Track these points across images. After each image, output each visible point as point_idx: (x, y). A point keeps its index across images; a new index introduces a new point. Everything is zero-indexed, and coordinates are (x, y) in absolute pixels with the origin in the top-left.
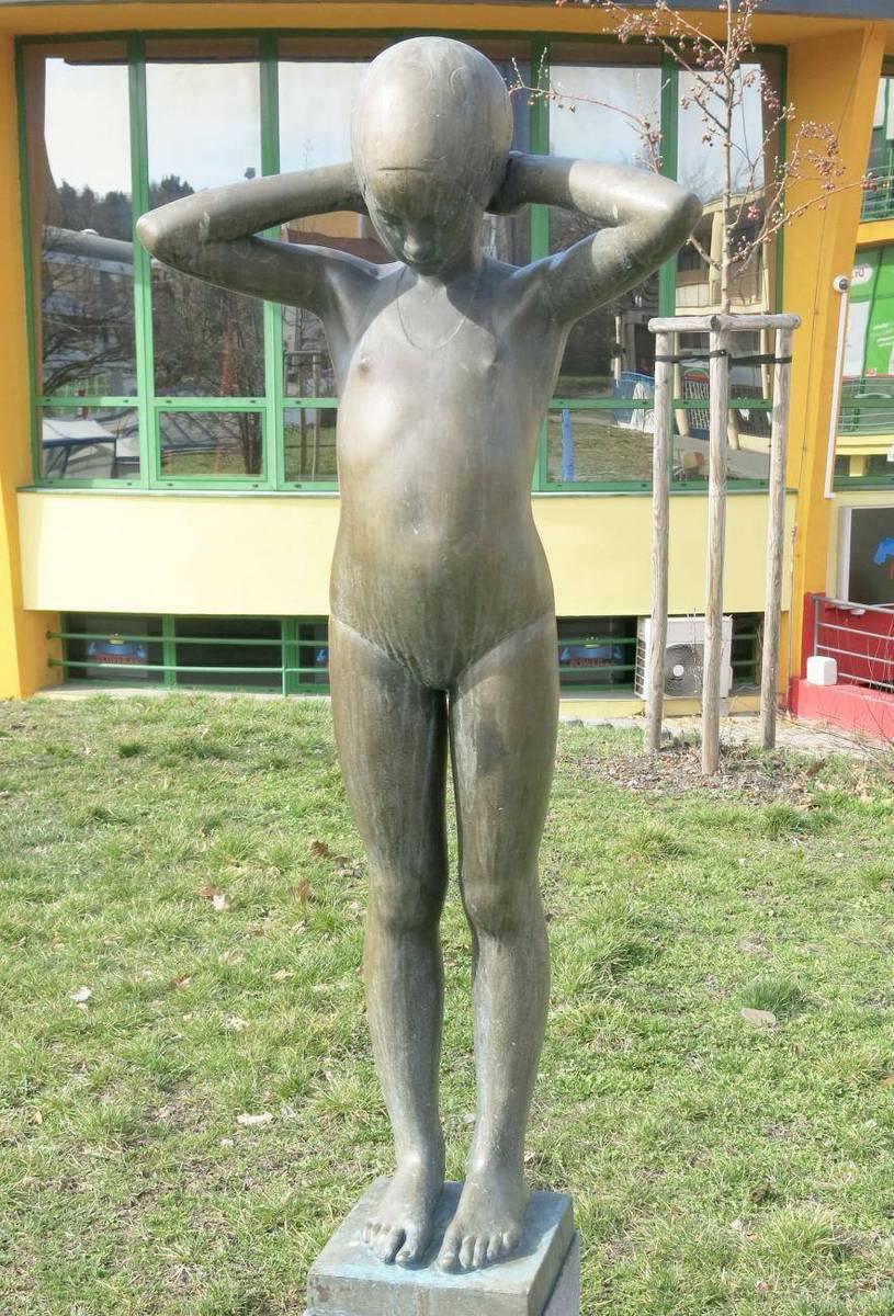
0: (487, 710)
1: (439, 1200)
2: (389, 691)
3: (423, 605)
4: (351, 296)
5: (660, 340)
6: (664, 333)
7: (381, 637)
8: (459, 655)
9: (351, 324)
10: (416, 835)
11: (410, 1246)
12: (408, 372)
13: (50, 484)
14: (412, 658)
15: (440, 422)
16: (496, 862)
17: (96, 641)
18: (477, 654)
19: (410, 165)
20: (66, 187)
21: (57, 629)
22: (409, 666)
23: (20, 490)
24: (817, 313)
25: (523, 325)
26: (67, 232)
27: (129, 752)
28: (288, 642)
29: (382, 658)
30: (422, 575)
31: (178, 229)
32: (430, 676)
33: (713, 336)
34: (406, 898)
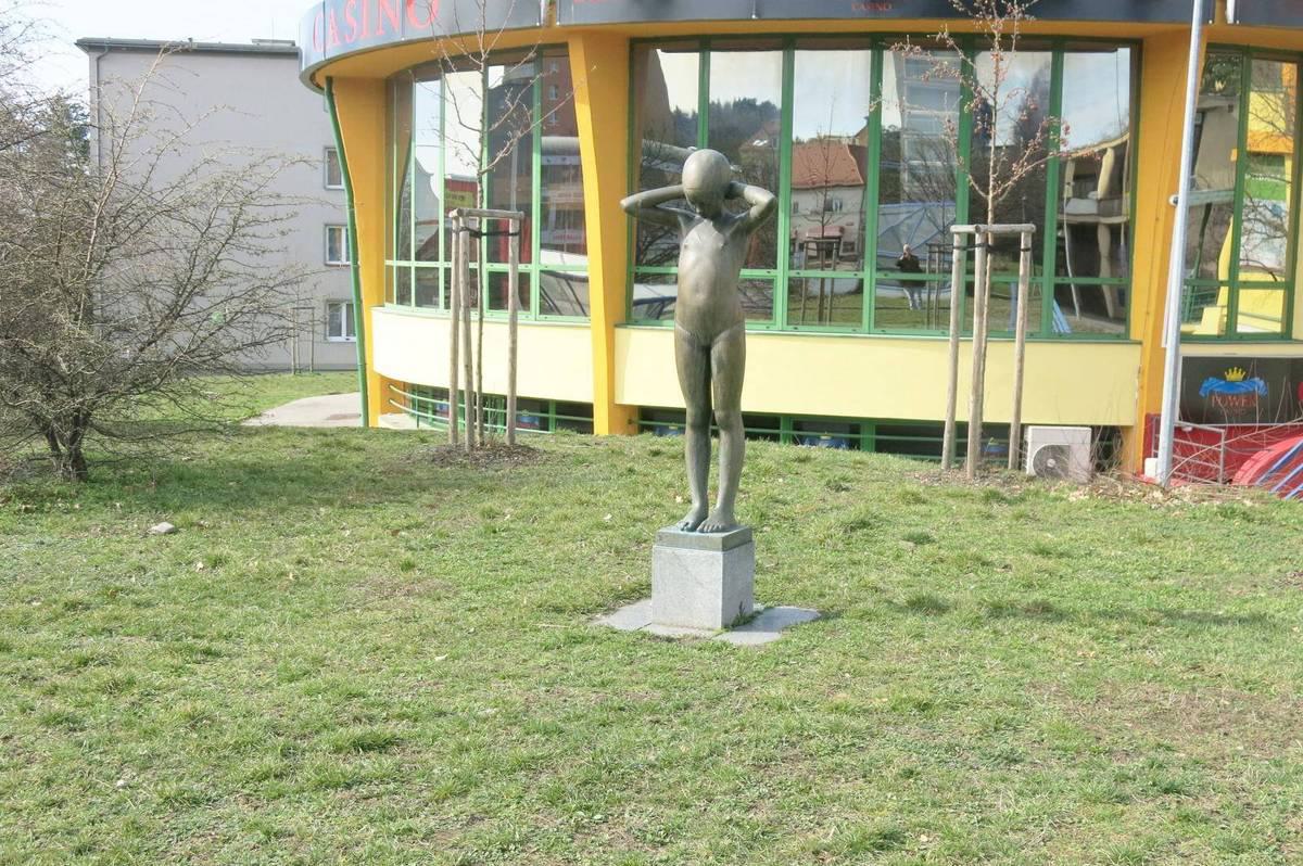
0: (720, 353)
1: (702, 516)
4: (685, 224)
5: (956, 237)
6: (958, 233)
9: (684, 234)
10: (699, 394)
11: (689, 526)
12: (699, 248)
13: (636, 323)
15: (707, 263)
17: (660, 426)
18: (717, 335)
20: (678, 111)
21: (635, 418)
23: (616, 326)
24: (1157, 219)
25: (734, 235)
26: (676, 148)
27: (656, 453)
28: (785, 432)
30: (699, 309)
32: (703, 342)
33: (977, 236)
34: (696, 416)
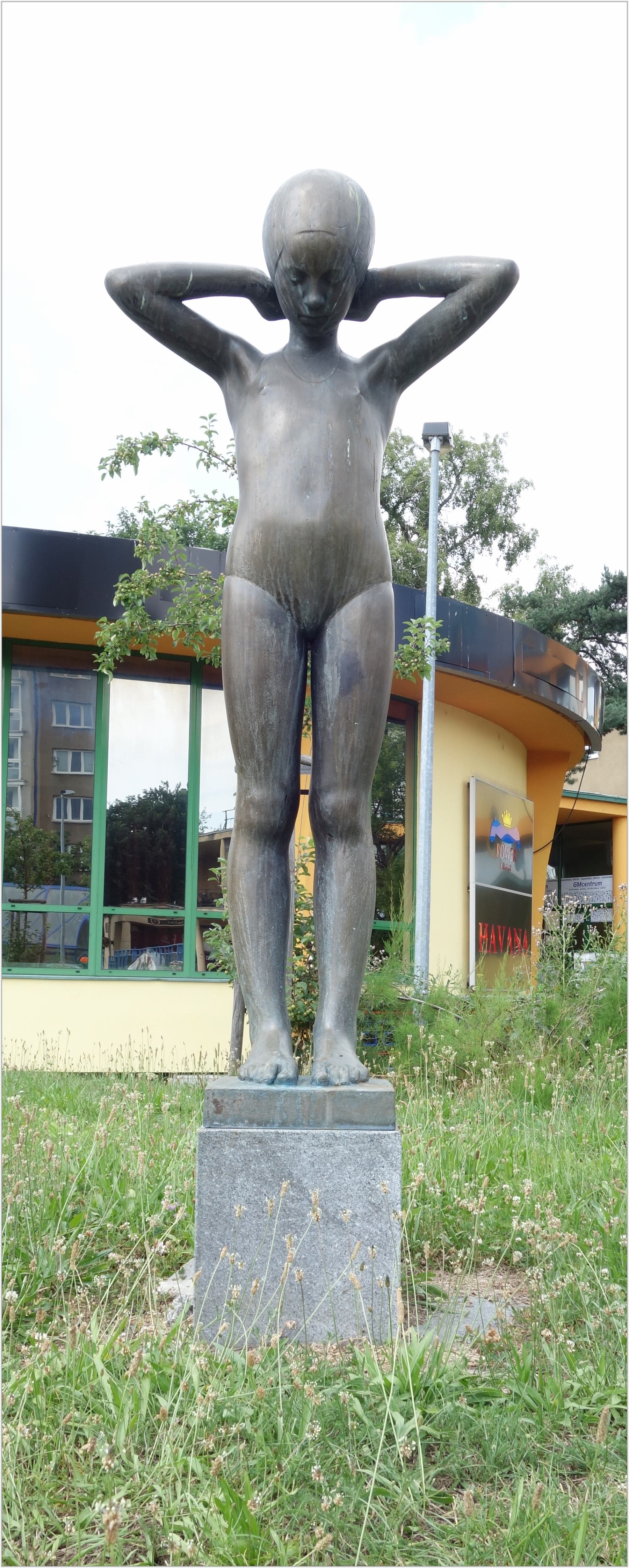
2: (276, 627)
3: (310, 553)
7: (273, 585)
8: (331, 599)
14: (296, 600)
16: (349, 771)
19: (322, 229)
22: (292, 609)
29: (273, 604)
31: (139, 278)
